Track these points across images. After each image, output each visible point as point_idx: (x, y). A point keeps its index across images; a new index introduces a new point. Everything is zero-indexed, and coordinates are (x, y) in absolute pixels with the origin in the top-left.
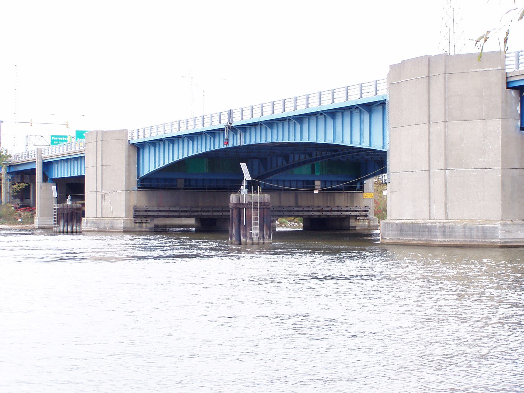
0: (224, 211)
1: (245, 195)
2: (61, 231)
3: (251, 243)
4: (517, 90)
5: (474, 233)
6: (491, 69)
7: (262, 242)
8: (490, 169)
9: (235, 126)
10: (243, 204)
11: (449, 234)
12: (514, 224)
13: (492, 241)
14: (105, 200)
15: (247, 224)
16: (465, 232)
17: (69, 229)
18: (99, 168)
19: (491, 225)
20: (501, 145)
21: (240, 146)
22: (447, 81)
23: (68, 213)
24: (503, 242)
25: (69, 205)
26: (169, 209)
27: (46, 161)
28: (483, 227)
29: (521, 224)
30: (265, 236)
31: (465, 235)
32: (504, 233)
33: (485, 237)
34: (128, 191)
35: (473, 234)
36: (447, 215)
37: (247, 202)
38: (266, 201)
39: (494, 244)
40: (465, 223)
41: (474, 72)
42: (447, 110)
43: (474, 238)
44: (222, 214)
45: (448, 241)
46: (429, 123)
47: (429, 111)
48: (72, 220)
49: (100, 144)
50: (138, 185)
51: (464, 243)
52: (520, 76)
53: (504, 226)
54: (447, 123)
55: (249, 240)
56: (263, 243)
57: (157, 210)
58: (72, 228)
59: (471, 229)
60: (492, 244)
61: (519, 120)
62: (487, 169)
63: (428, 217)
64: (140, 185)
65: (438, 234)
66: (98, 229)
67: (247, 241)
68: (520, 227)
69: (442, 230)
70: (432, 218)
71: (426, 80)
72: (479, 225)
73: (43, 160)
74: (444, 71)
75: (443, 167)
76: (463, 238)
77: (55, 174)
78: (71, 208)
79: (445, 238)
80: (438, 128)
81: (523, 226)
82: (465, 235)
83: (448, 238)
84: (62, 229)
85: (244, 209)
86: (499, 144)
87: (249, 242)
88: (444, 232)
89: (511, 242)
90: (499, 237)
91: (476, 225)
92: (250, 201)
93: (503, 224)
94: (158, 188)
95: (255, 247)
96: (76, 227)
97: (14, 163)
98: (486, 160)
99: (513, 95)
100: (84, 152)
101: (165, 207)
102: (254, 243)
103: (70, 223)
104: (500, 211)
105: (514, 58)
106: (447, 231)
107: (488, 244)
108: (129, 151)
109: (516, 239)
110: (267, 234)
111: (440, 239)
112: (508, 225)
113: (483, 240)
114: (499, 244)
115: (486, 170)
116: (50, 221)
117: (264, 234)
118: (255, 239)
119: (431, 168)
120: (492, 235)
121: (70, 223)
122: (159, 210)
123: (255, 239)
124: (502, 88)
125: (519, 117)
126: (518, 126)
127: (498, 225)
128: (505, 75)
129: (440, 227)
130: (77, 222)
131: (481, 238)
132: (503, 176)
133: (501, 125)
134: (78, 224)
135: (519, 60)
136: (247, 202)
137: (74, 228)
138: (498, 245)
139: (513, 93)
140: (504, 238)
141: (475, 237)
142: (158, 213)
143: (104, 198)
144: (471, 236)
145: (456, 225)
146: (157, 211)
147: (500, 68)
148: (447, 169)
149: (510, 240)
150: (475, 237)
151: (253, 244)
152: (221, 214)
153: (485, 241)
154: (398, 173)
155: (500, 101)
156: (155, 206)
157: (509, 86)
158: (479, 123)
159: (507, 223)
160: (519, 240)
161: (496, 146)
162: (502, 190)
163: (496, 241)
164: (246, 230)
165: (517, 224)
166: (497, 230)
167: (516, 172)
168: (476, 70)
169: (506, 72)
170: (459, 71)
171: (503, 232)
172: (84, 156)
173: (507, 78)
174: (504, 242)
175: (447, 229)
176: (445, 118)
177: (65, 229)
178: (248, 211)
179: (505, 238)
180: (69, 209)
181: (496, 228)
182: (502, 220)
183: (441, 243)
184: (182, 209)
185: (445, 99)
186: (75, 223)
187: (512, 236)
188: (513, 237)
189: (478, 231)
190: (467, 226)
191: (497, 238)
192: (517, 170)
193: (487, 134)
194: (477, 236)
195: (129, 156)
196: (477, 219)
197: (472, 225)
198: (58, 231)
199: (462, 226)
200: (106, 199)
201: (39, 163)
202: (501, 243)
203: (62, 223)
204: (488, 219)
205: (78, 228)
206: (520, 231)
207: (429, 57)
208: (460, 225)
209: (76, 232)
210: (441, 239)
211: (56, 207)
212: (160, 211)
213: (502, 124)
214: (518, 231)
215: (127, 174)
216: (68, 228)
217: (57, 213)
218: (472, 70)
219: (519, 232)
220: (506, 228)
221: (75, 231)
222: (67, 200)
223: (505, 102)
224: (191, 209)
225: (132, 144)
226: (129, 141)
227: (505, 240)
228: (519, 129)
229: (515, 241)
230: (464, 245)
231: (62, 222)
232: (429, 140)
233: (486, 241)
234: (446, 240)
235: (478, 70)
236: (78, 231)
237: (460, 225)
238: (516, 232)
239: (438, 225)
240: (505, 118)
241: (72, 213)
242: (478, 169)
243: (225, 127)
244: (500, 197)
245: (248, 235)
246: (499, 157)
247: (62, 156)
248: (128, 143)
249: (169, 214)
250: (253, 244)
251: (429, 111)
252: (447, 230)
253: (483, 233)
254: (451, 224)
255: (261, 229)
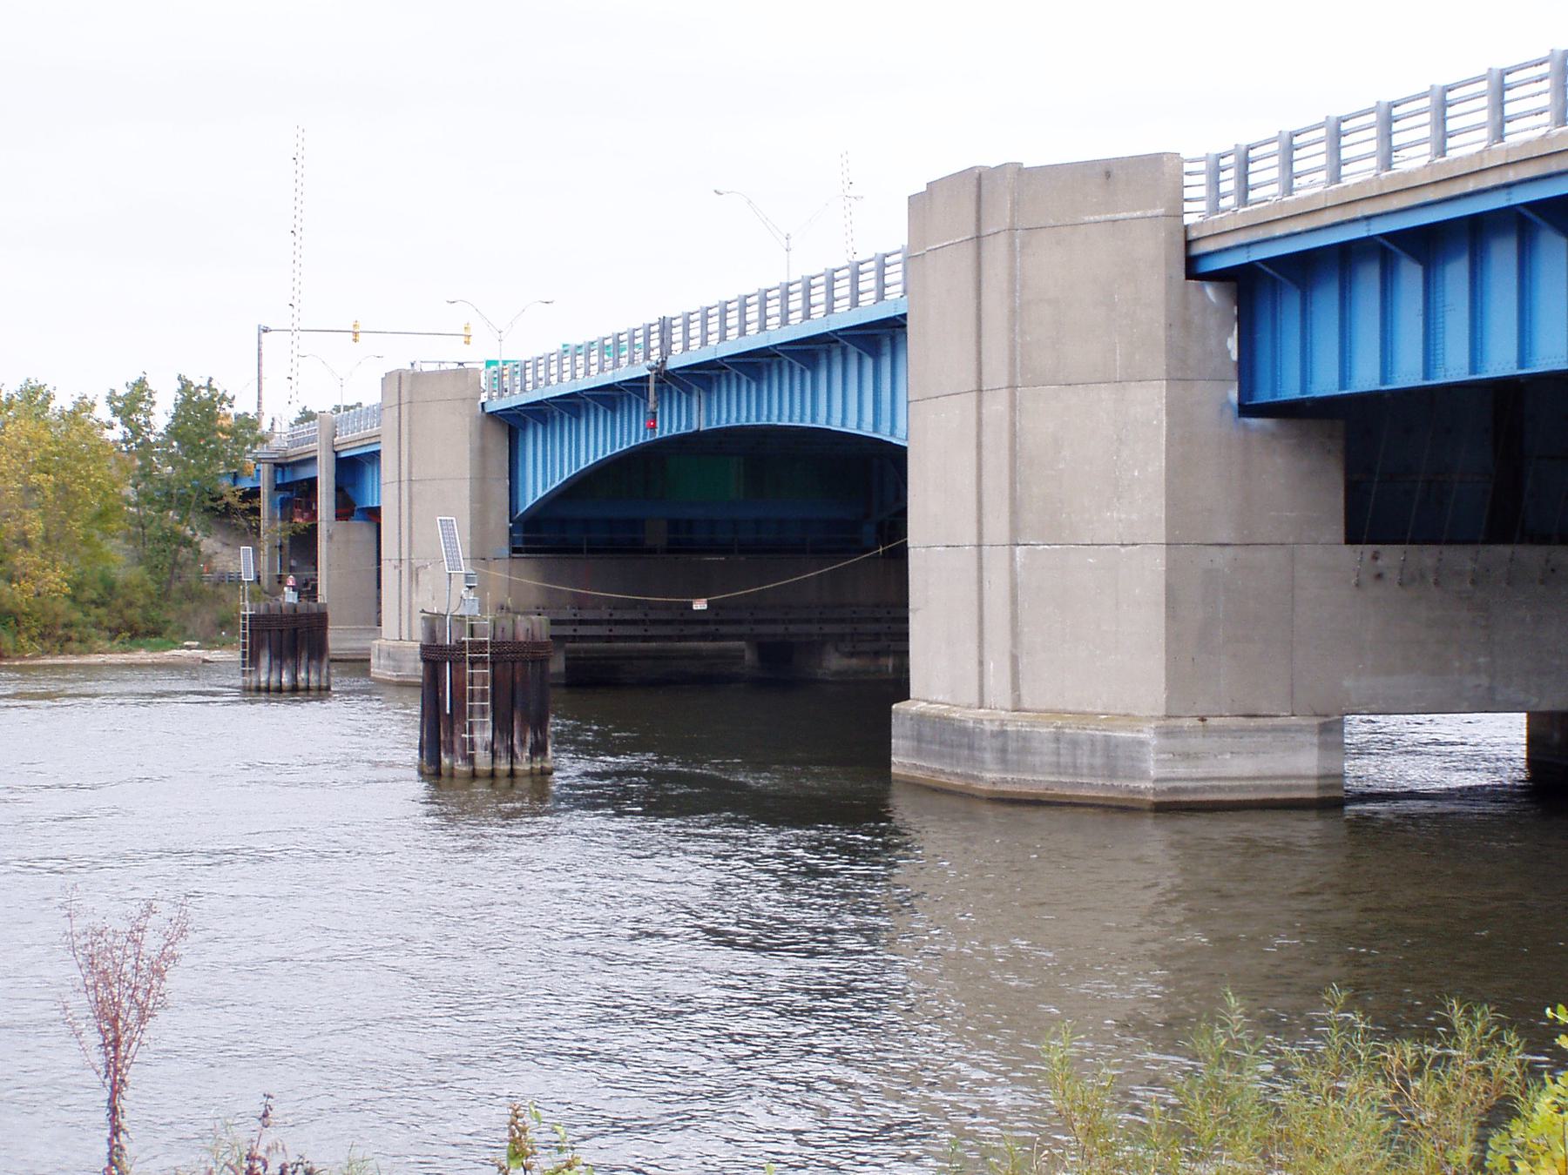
0: (791, 622)
1: (448, 618)
2: (263, 685)
3: (466, 772)
4: (1223, 284)
5: (1084, 760)
6: (1139, 213)
7: (508, 767)
8: (1134, 547)
9: (674, 370)
10: (441, 647)
11: (1015, 757)
12: (1208, 732)
13: (1132, 785)
14: (420, 588)
15: (454, 713)
16: (1059, 754)
17: (286, 679)
18: (405, 485)
19: (1129, 735)
20: (1164, 468)
21: (698, 431)
22: (1018, 255)
23: (281, 631)
24: (1163, 791)
25: (286, 607)
26: (611, 615)
27: (343, 455)
28: (1107, 739)
29: (1234, 728)
30: (517, 749)
31: (1058, 765)
32: (1169, 760)
33: (1113, 773)
34: (480, 557)
35: (1079, 761)
36: (1019, 696)
37: (453, 643)
38: (522, 638)
39: (1137, 797)
40: (1060, 723)
41: (1090, 223)
42: (1018, 348)
43: (1082, 775)
44: (786, 629)
45: (1015, 783)
46: (980, 390)
47: (979, 353)
48: (295, 655)
49: (404, 408)
50: (512, 540)
51: (1057, 791)
52: (1215, 238)
53: (1168, 738)
54: (1018, 394)
55: (460, 763)
56: (512, 774)
57: (573, 618)
58: (295, 677)
59: (1074, 743)
60: (1131, 796)
61: (1236, 384)
62: (1127, 545)
63: (975, 700)
64: (521, 540)
65: (988, 756)
66: (398, 676)
67: (456, 767)
68: (1229, 740)
69: (997, 743)
70: (988, 700)
71: (969, 250)
72: (1097, 733)
73: (336, 453)
74: (1008, 220)
75: (1006, 540)
76: (1053, 773)
77: (373, 497)
78: (291, 616)
79: (1006, 771)
80: (996, 406)
81: (1241, 738)
82: (1058, 765)
83: (1013, 771)
84: (263, 678)
85: (448, 664)
86: (1157, 465)
87: (464, 769)
88: (1004, 751)
89: (1195, 790)
90: (1152, 772)
91: (1088, 732)
92: (463, 639)
93: (1164, 730)
94: (580, 551)
95: (481, 788)
96: (308, 672)
97: (287, 458)
98: (1123, 516)
99: (1209, 300)
100: (377, 440)
101: (599, 608)
102: (477, 773)
103: (289, 661)
104: (1163, 686)
105: (1202, 179)
106: (1010, 750)
107: (1120, 796)
108: (483, 434)
109: (1219, 779)
110: (523, 742)
111: (991, 776)
112: (1185, 732)
113: (1108, 784)
114: (1151, 798)
115: (1123, 550)
116: (359, 639)
117: (515, 742)
118: (483, 760)
119: (986, 541)
120: (1133, 766)
121: (289, 661)
122: (578, 618)
123: (483, 760)
124: (1171, 277)
125: (1232, 373)
126: (1228, 402)
127: (1148, 734)
128: (1183, 234)
129: (994, 735)
130: (309, 659)
131: (1103, 776)
132: (1170, 570)
133: (1164, 401)
134: (314, 663)
135: (1221, 184)
136: (453, 643)
137: (302, 675)
138: (1149, 801)
139: (1210, 290)
140: (1169, 775)
141: (1085, 771)
142: (574, 627)
143: (417, 582)
144: (1075, 767)
145: (1036, 729)
146: (572, 622)
147: (1161, 211)
148: (1018, 545)
149: (1191, 784)
150: (1085, 771)
151: (474, 776)
152: (780, 629)
153: (1113, 785)
154: (923, 550)
155: (1163, 321)
156: (568, 607)
157: (1193, 268)
158: (1106, 393)
159: (1182, 727)
160: (1237, 783)
161: (1150, 470)
162: (1167, 617)
163: (1143, 787)
164: (452, 733)
165: (1221, 731)
166: (1145, 749)
167: (1221, 558)
168: (1097, 218)
169: (1186, 223)
170: (1052, 222)
171: (1163, 756)
172: (377, 453)
173: (1188, 243)
174: (1169, 789)
175: (1010, 742)
176: (1012, 375)
177: (274, 679)
178: (457, 671)
179: (1174, 775)
180: (286, 616)
181: (1142, 743)
182: (1168, 717)
183: (996, 789)
184: (652, 617)
185: (1013, 312)
186: (304, 661)
187: (1199, 770)
188: (1202, 775)
189: (1093, 752)
190: (1063, 733)
191: (1144, 775)
192: (1228, 550)
193: (1127, 430)
194: (1092, 767)
195: (482, 453)
196: (1099, 710)
197: (1079, 731)
198: (254, 684)
199: (1050, 732)
200: (420, 583)
201: (324, 461)
202: (1156, 793)
203: (265, 661)
204: (1129, 711)
205: (313, 678)
206: (1232, 753)
207: (980, 175)
208: (1045, 730)
209: (308, 689)
210: (995, 775)
211: (248, 613)
212: (582, 622)
213: (1166, 397)
214: (1221, 754)
215: (478, 506)
216: (281, 677)
217: (250, 630)
218: (1086, 219)
219: (1228, 756)
220: (1177, 744)
221: (302, 684)
222: (286, 589)
223: (1180, 323)
224: (717, 614)
225: (492, 413)
226: (483, 404)
227: (1171, 784)
228: (1232, 412)
229: (1212, 787)
230: (1056, 795)
231: (265, 656)
232: (979, 446)
233: (1115, 784)
234: (1009, 777)
235: (1103, 217)
236: (313, 684)
237: (1045, 730)
238: (1216, 756)
239: (988, 727)
240: (1179, 375)
241: (295, 630)
242: (1102, 547)
243: (649, 372)
244: (1162, 641)
245: (457, 746)
246: (1157, 508)
247: (358, 444)
248: (480, 409)
249: (575, 630)
250: (474, 776)
251: (979, 353)
252: (1012, 745)
253: (1108, 757)
254: (1022, 726)
255: (502, 726)
